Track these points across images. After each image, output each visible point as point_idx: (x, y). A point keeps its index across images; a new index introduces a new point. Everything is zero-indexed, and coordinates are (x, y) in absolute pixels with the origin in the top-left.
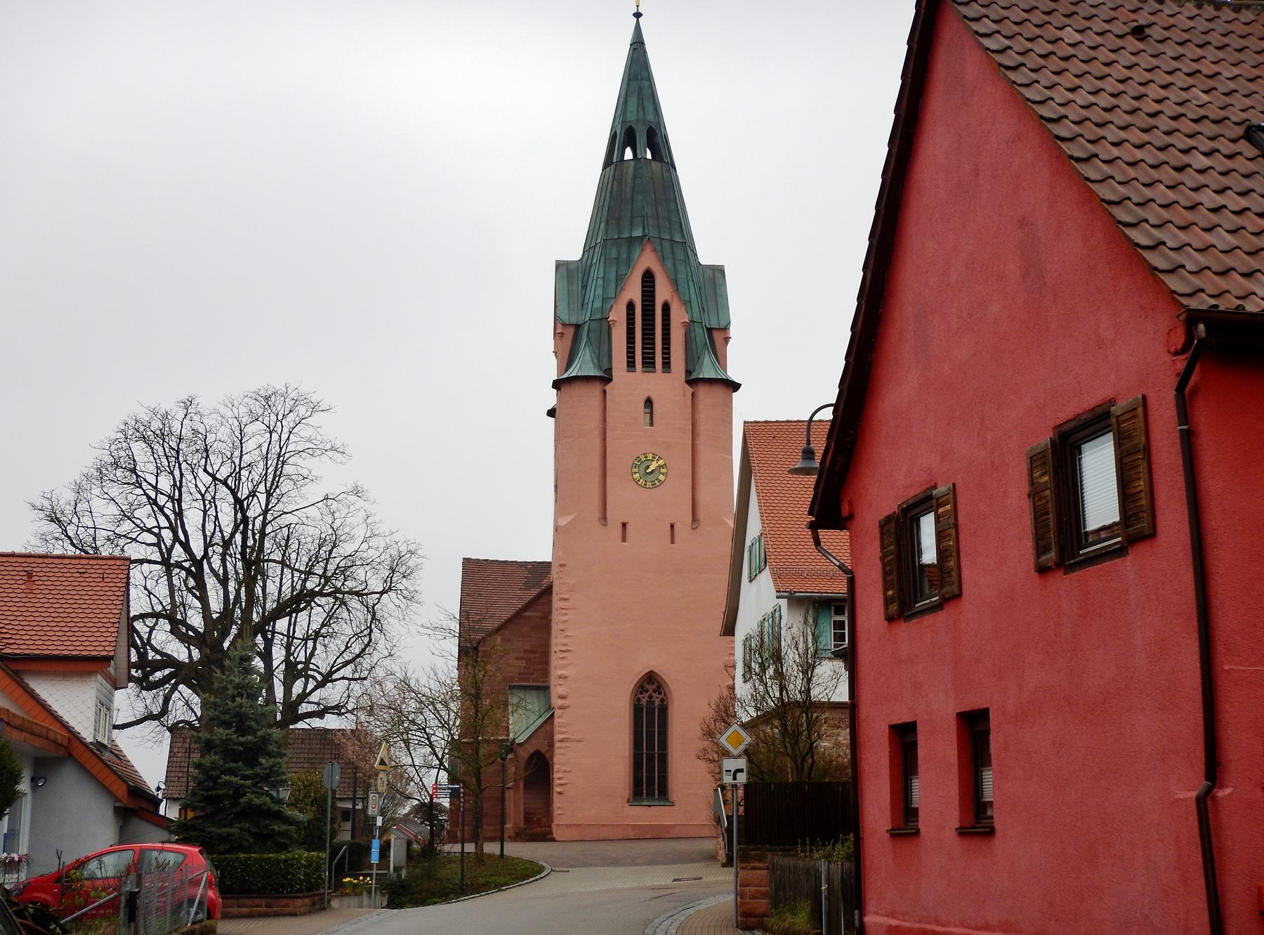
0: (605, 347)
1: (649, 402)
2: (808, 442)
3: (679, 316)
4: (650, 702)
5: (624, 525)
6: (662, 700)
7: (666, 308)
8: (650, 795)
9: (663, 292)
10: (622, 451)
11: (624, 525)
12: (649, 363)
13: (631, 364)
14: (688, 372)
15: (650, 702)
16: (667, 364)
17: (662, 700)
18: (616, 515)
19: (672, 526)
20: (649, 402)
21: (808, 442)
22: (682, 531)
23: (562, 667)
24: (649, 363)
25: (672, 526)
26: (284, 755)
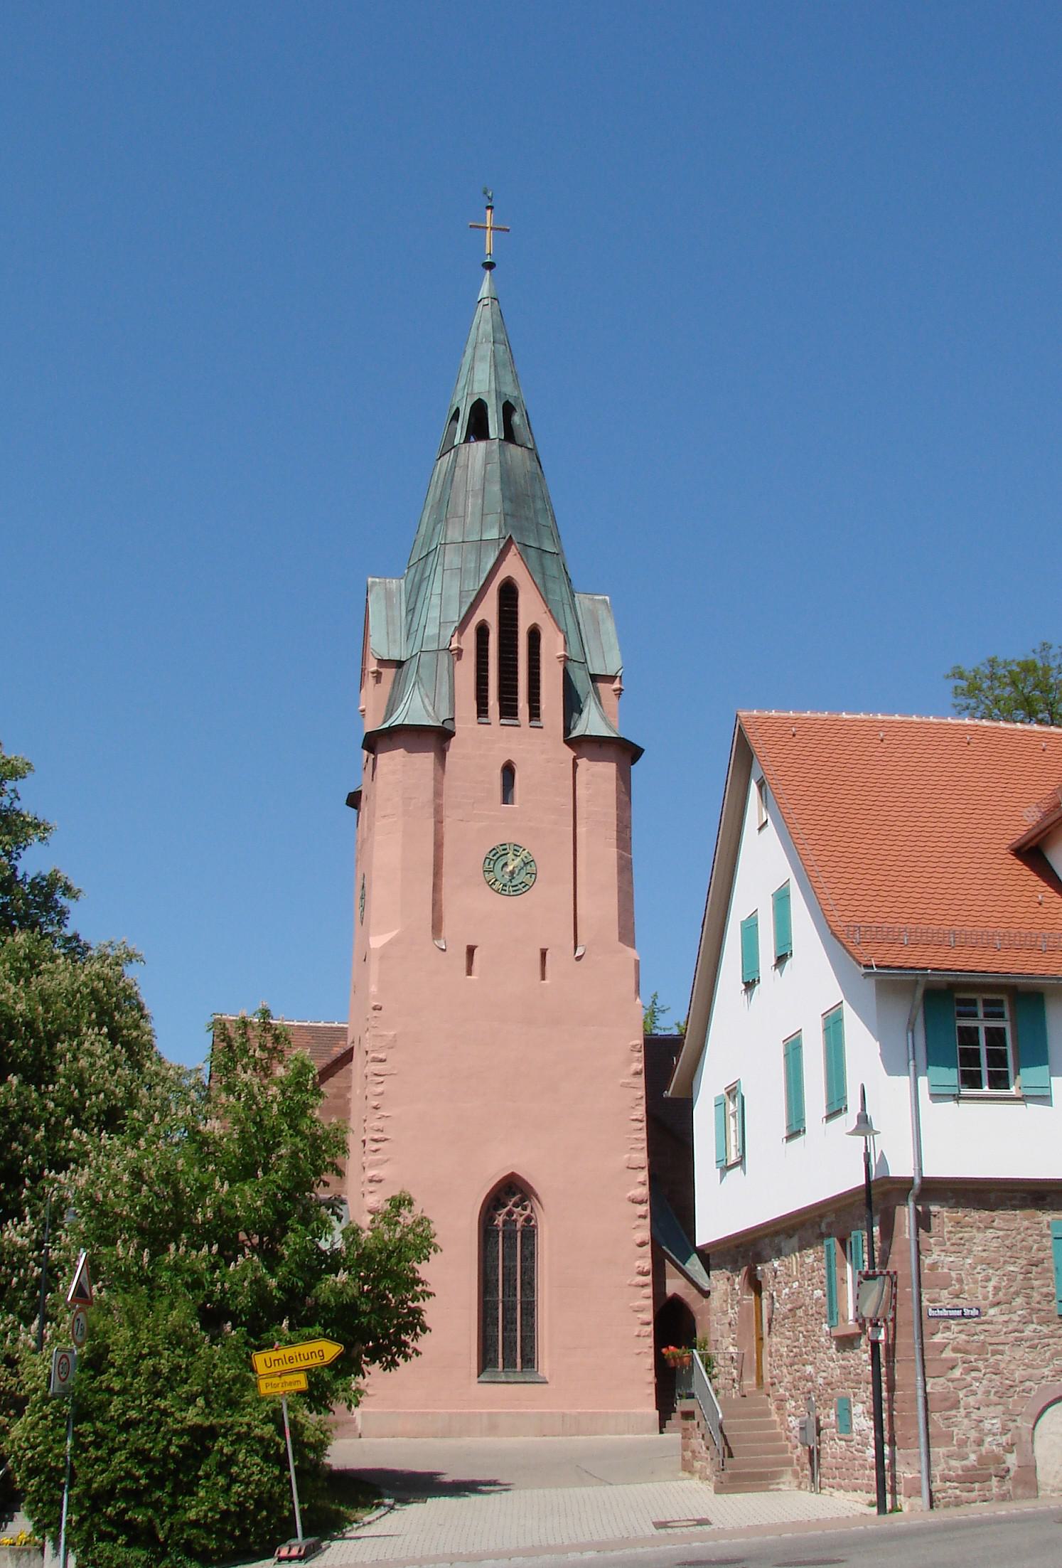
0: (445, 689)
1: (508, 771)
2: (864, 1109)
3: (552, 647)
4: (509, 1222)
5: (471, 951)
6: (528, 1219)
7: (534, 635)
8: (509, 1363)
9: (530, 611)
10: (466, 851)
11: (471, 951)
12: (508, 710)
13: (482, 710)
14: (567, 730)
15: (509, 1222)
16: (535, 713)
17: (528, 1219)
18: (456, 933)
19: (544, 953)
20: (508, 771)
21: (864, 1109)
22: (559, 961)
23: (375, 1164)
24: (508, 710)
25: (544, 953)
26: (80, 1159)
